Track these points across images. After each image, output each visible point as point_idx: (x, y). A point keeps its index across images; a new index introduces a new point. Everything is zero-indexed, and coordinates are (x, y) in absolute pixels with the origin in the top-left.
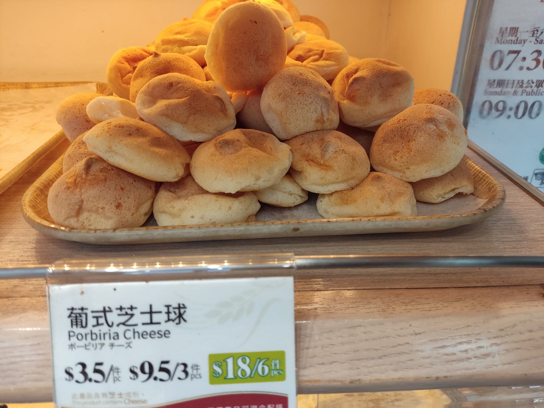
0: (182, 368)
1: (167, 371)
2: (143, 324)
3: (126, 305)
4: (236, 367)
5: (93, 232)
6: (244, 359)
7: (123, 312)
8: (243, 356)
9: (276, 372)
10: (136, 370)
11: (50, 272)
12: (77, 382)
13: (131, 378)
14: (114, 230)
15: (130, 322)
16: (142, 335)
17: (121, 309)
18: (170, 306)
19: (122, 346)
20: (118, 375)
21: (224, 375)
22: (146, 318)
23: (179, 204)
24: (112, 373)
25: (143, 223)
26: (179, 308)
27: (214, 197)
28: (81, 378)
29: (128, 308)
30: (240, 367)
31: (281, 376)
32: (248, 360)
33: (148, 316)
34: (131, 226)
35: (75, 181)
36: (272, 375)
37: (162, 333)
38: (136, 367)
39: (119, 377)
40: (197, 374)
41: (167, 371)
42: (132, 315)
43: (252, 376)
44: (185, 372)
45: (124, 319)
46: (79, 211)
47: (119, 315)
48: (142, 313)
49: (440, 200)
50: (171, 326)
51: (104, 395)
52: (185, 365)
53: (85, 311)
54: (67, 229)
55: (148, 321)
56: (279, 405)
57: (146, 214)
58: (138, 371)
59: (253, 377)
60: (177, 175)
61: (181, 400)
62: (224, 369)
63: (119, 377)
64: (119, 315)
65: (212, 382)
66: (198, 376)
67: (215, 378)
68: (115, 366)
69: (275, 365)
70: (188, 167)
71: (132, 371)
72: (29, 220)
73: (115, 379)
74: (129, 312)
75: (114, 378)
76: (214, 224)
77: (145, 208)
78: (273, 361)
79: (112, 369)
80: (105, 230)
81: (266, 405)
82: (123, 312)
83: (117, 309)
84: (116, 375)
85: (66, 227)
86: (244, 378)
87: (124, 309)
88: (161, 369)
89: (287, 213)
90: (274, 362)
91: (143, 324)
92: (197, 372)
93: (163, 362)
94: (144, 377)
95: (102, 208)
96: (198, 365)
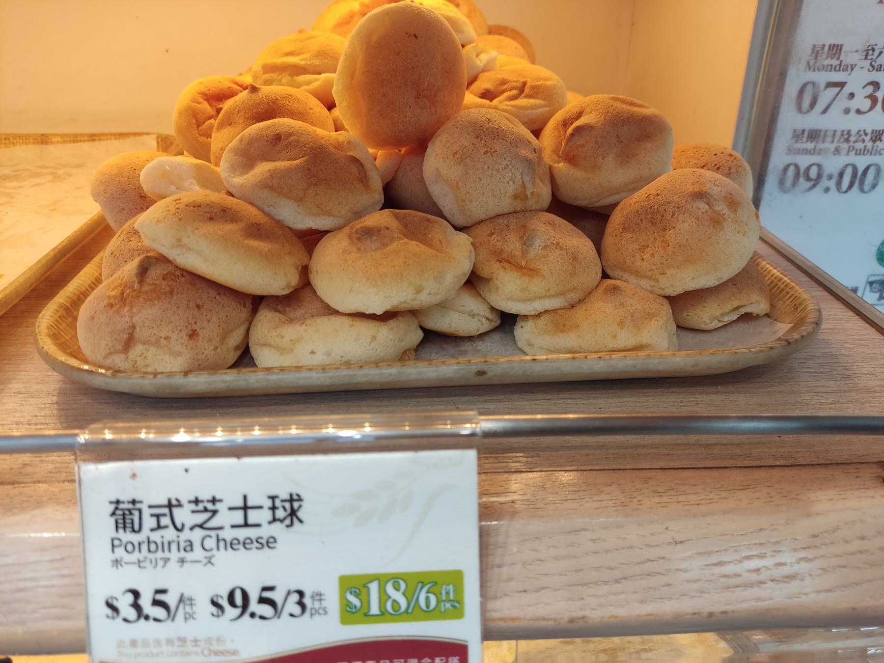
0: (295, 597)
1: (271, 603)
2: (233, 526)
3: (205, 496)
4: (383, 596)
5: (152, 376)
6: (396, 584)
7: (201, 507)
8: (395, 579)
9: (448, 605)
10: (220, 602)
11: (81, 442)
12: (125, 620)
13: (213, 615)
14: (186, 374)
15: (212, 524)
16: (231, 544)
17: (197, 501)
18: (277, 497)
19: (199, 561)
20: (192, 609)
21: (365, 610)
22: (238, 517)
23: (290, 332)
24: (181, 606)
25: (233, 362)
26: (291, 500)
27: (347, 321)
28: (132, 614)
29: (208, 501)
30: (389, 597)
31: (456, 610)
32: (403, 586)
33: (241, 513)
34: (212, 368)
35: (122, 294)
36: (443, 609)
37: (264, 541)
38: (222, 597)
39: (194, 613)
40: (319, 608)
41: (271, 603)
42: (215, 512)
43: (410, 611)
44: (301, 604)
45: (201, 518)
46: (128, 343)
47: (193, 512)
48: (231, 509)
49: (715, 324)
50: (277, 530)
51: (169, 642)
52: (301, 594)
53: (138, 506)
54: (109, 373)
55: (241, 521)
56: (453, 658)
57: (237, 348)
58: (224, 603)
59: (412, 613)
60: (288, 285)
61: (295, 650)
62: (364, 599)
63: (194, 613)
64: (193, 512)
65: (344, 621)
66: (321, 611)
67: (350, 614)
68: (187, 594)
69: (448, 593)
70: (305, 271)
71: (214, 603)
72: (48, 358)
73: (187, 616)
74: (210, 506)
75: (185, 613)
76: (348, 364)
77: (235, 338)
78: (444, 587)
79: (181, 600)
80: (171, 374)
81: (432, 658)
82: (201, 507)
83: (190, 502)
84: (188, 609)
85: (107, 369)
86: (397, 615)
87: (202, 501)
88: (262, 600)
89: (467, 346)
90: (446, 589)
91: (233, 526)
92: (321, 604)
93: (265, 589)
94: (234, 612)
95: (167, 338)
96: (322, 593)
